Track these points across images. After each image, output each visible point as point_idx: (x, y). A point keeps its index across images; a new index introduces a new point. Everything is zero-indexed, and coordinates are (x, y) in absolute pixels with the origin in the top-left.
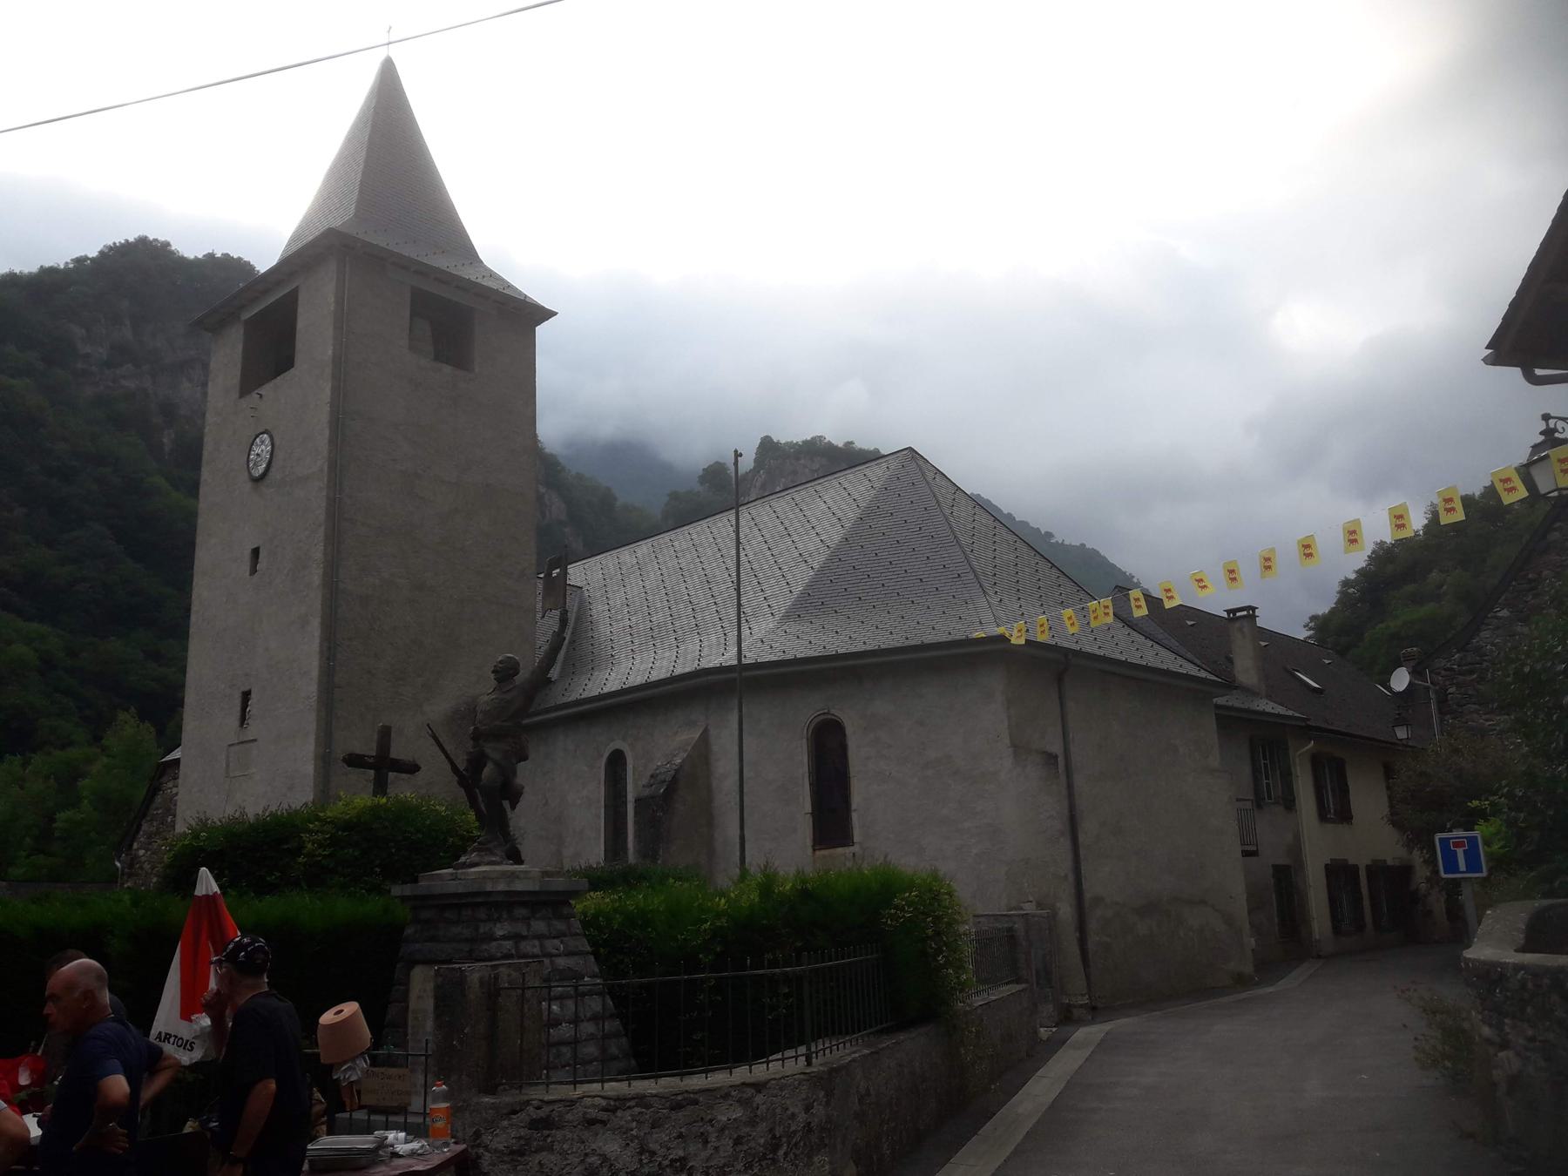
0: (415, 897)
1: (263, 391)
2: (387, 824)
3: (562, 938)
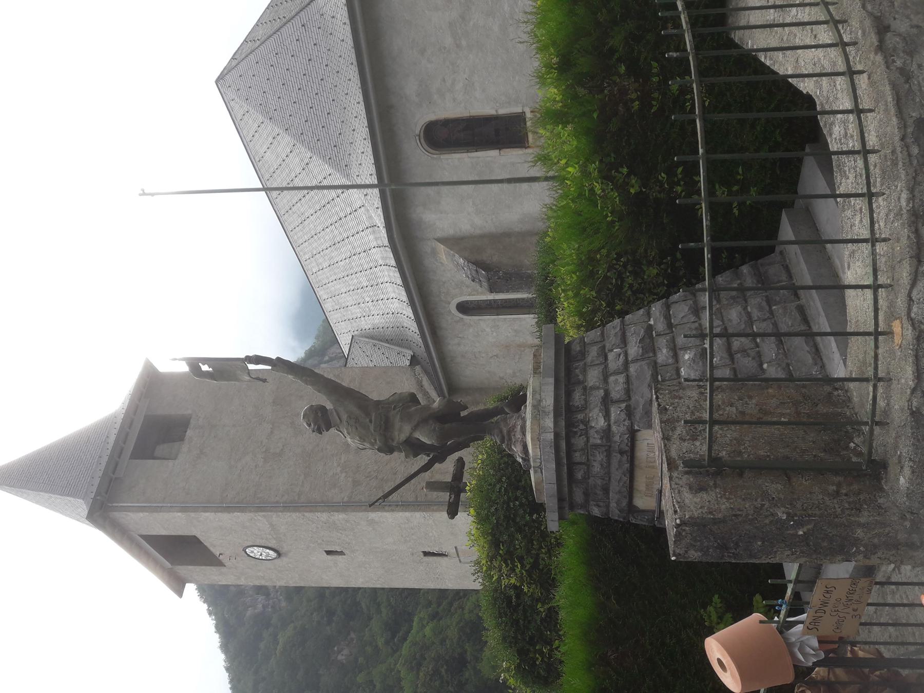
0: (561, 509)
1: (217, 554)
2: (493, 509)
3: (607, 351)
